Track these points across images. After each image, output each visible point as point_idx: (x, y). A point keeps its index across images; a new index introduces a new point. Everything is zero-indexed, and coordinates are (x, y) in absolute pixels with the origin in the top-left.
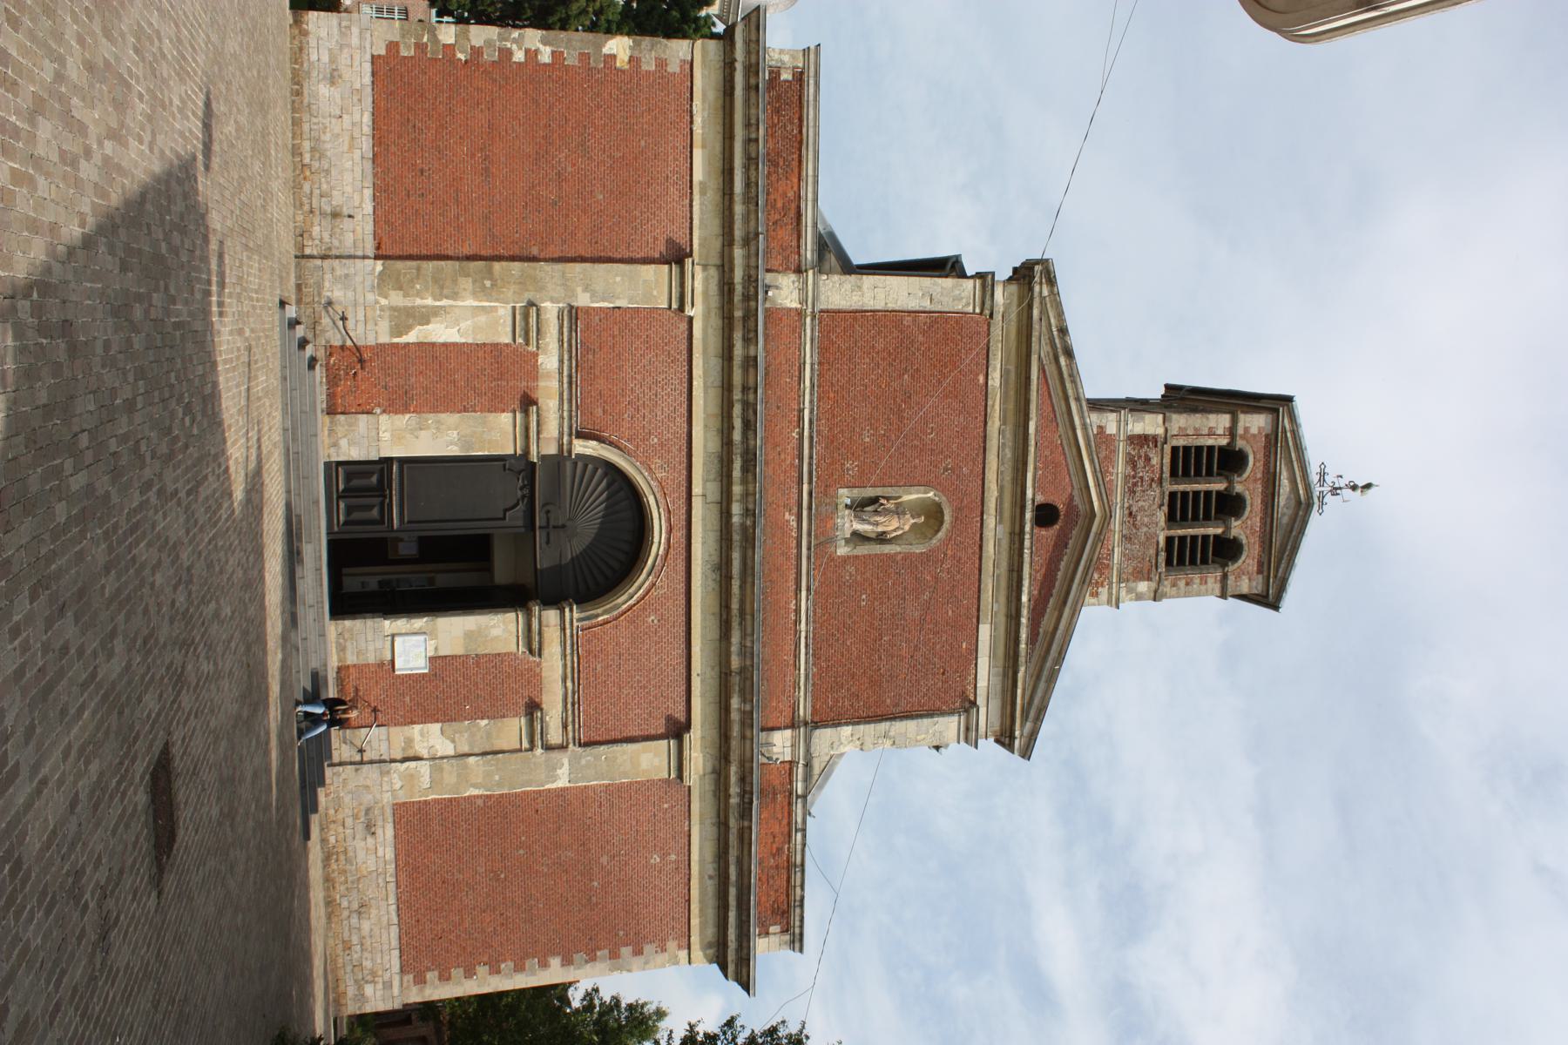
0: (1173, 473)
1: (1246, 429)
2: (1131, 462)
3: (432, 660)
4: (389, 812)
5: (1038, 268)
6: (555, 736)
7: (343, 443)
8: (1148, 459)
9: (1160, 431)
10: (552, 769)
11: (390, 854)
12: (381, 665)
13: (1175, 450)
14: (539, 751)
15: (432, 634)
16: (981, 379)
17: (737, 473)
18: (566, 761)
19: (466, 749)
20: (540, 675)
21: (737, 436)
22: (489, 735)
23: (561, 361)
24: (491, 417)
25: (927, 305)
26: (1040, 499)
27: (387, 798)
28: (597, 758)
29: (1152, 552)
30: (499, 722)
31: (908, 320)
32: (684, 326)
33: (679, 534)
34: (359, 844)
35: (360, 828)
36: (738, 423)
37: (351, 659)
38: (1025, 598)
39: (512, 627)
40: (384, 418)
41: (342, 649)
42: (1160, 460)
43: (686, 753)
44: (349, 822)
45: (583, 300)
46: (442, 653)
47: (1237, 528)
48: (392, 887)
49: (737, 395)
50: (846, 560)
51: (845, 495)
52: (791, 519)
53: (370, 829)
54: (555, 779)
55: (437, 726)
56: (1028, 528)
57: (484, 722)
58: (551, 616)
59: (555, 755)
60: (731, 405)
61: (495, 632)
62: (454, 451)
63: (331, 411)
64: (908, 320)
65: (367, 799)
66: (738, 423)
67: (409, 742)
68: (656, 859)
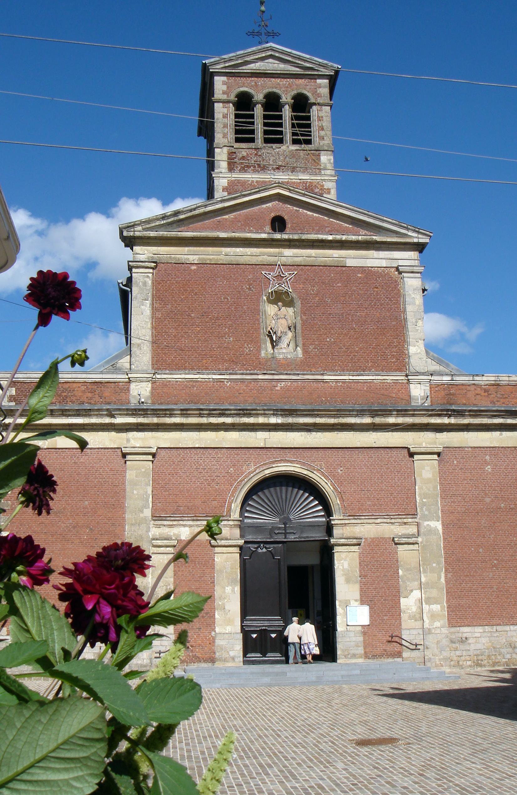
0: (252, 140)
1: (224, 93)
2: (244, 169)
3: (362, 602)
4: (453, 630)
5: (125, 234)
6: (413, 530)
7: (232, 654)
8: (243, 158)
9: (225, 150)
10: (431, 531)
11: (479, 629)
12: (364, 633)
13: (238, 140)
14: (420, 540)
15: (346, 604)
16: (194, 267)
17: (251, 420)
18: (426, 523)
19: (416, 583)
20: (373, 539)
21: (229, 420)
22: (408, 570)
23: (184, 526)
24: (217, 567)
25: (148, 303)
26: (268, 228)
27: (445, 631)
28: (424, 504)
29: (302, 153)
30: (401, 563)
31: (159, 315)
32: (163, 453)
33: (289, 455)
34: (472, 647)
35: (462, 647)
36: (221, 420)
37: (361, 650)
38: (330, 238)
39: (343, 555)
40: (217, 630)
41: (354, 656)
42: (244, 149)
43: (423, 450)
44: (458, 653)
45: (148, 513)
46: (358, 597)
47: (286, 98)
48: (499, 628)
49: (204, 420)
50: (305, 351)
51: (267, 350)
52: (279, 386)
53: (464, 641)
54: (436, 529)
55: (403, 601)
56: (285, 236)
57: (401, 572)
58: (336, 532)
59: (422, 530)
60: (211, 424)
61: (346, 566)
62: (237, 589)
63: (212, 660)
64: (159, 315)
65: (445, 642)
66: (221, 420)
67: (412, 617)
68: (489, 468)
